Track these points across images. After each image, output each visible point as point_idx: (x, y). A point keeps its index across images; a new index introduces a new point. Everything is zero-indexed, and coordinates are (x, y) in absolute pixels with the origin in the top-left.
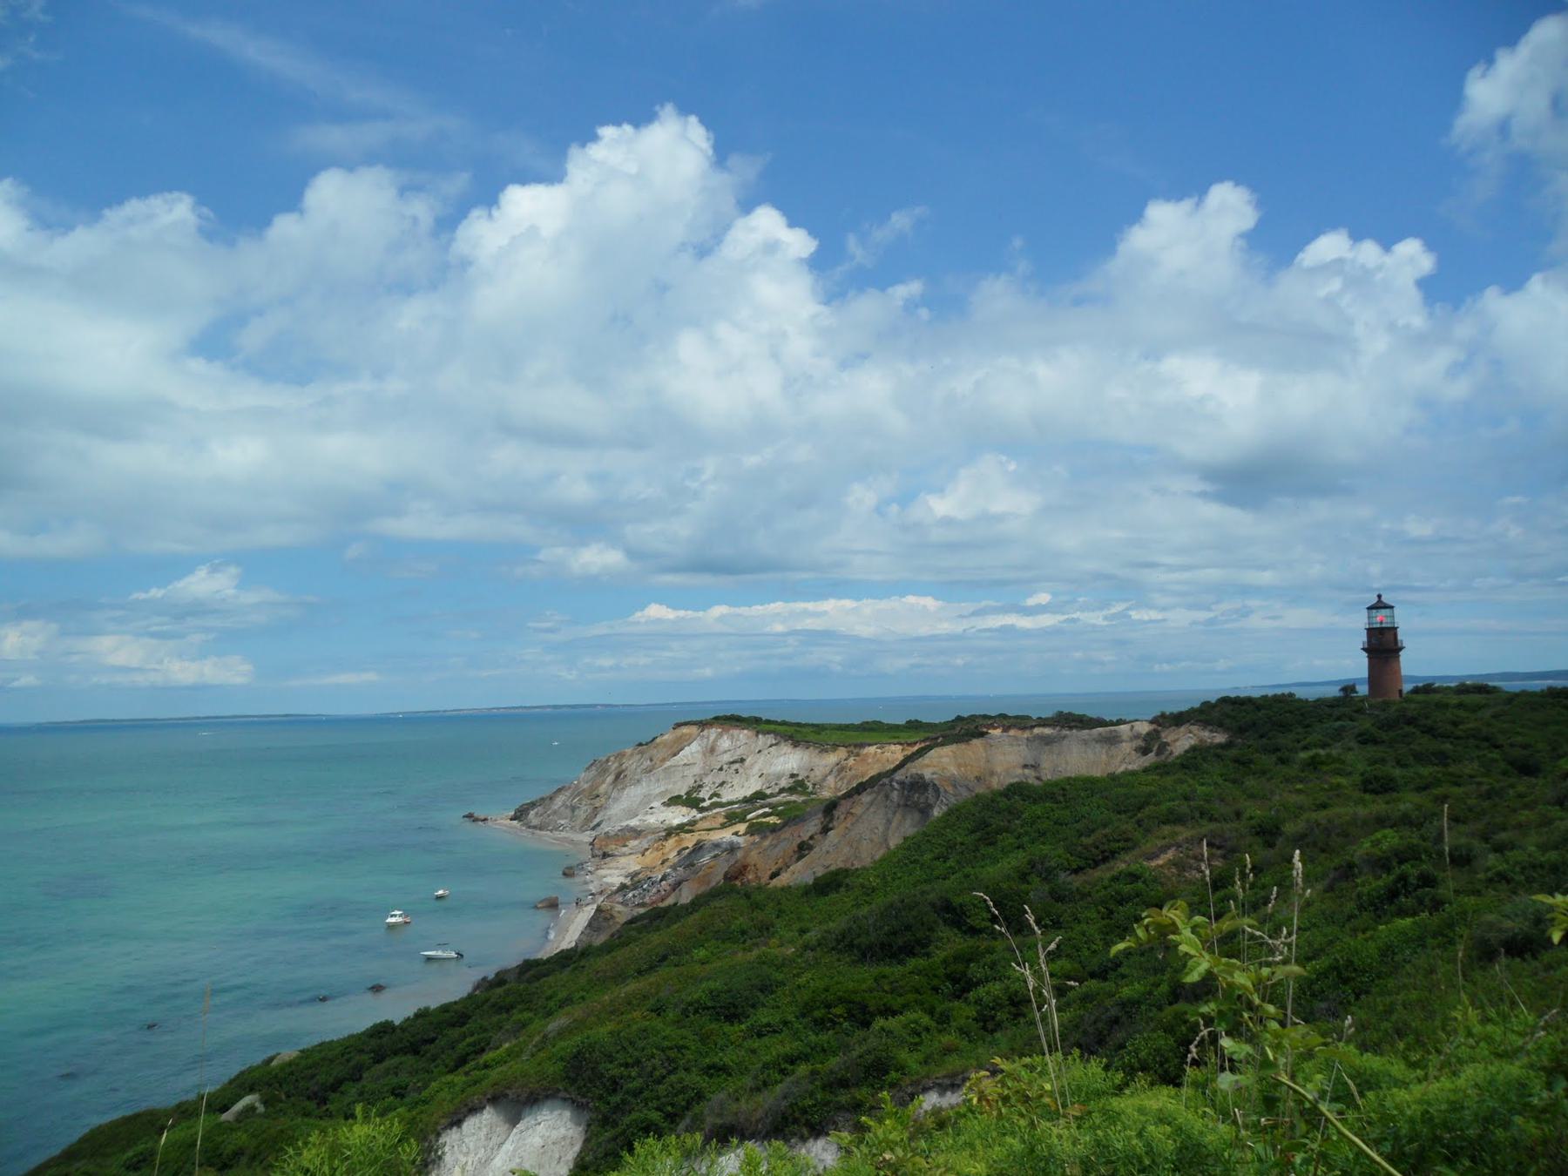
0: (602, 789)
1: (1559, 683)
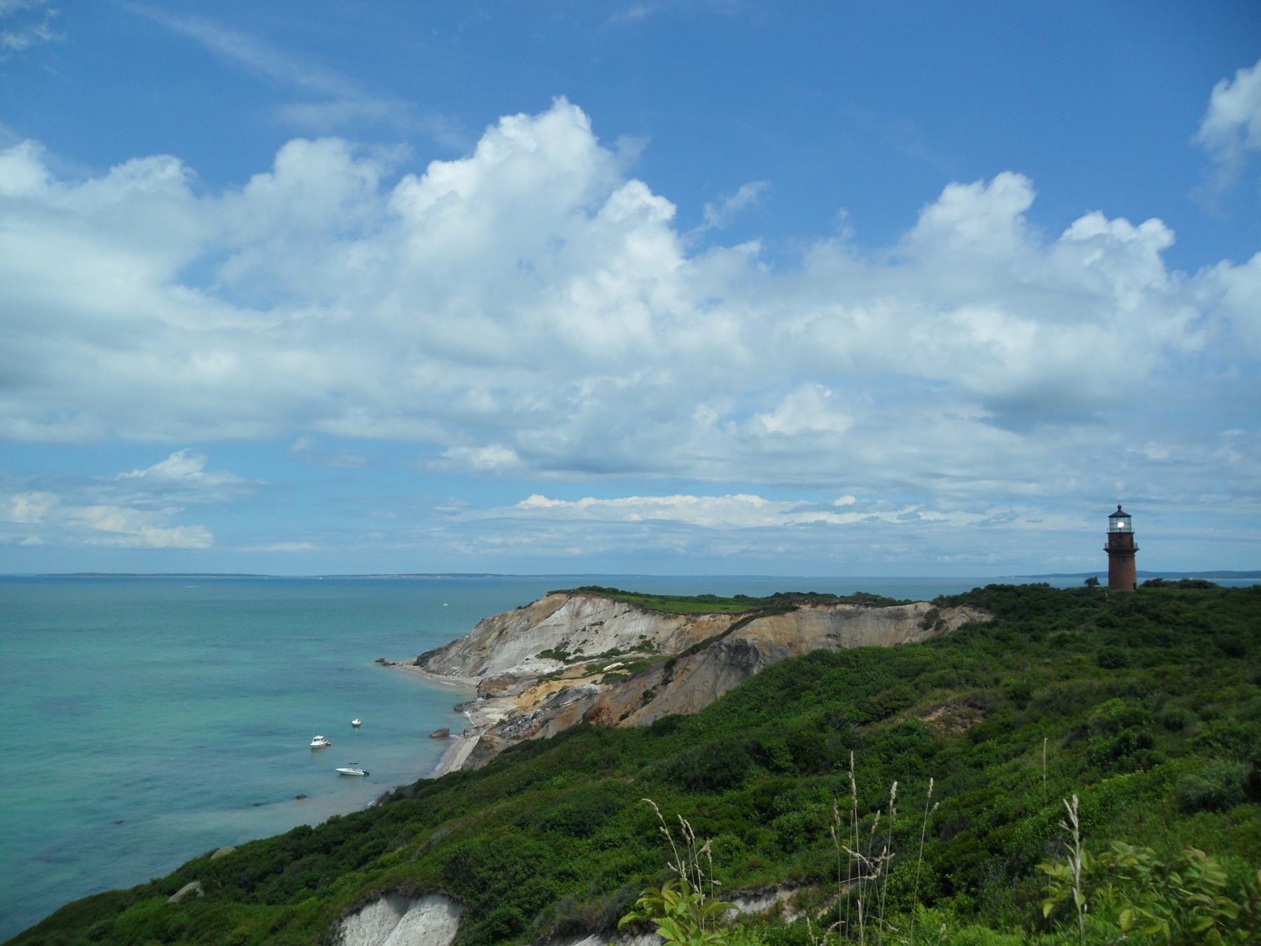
0: (488, 643)
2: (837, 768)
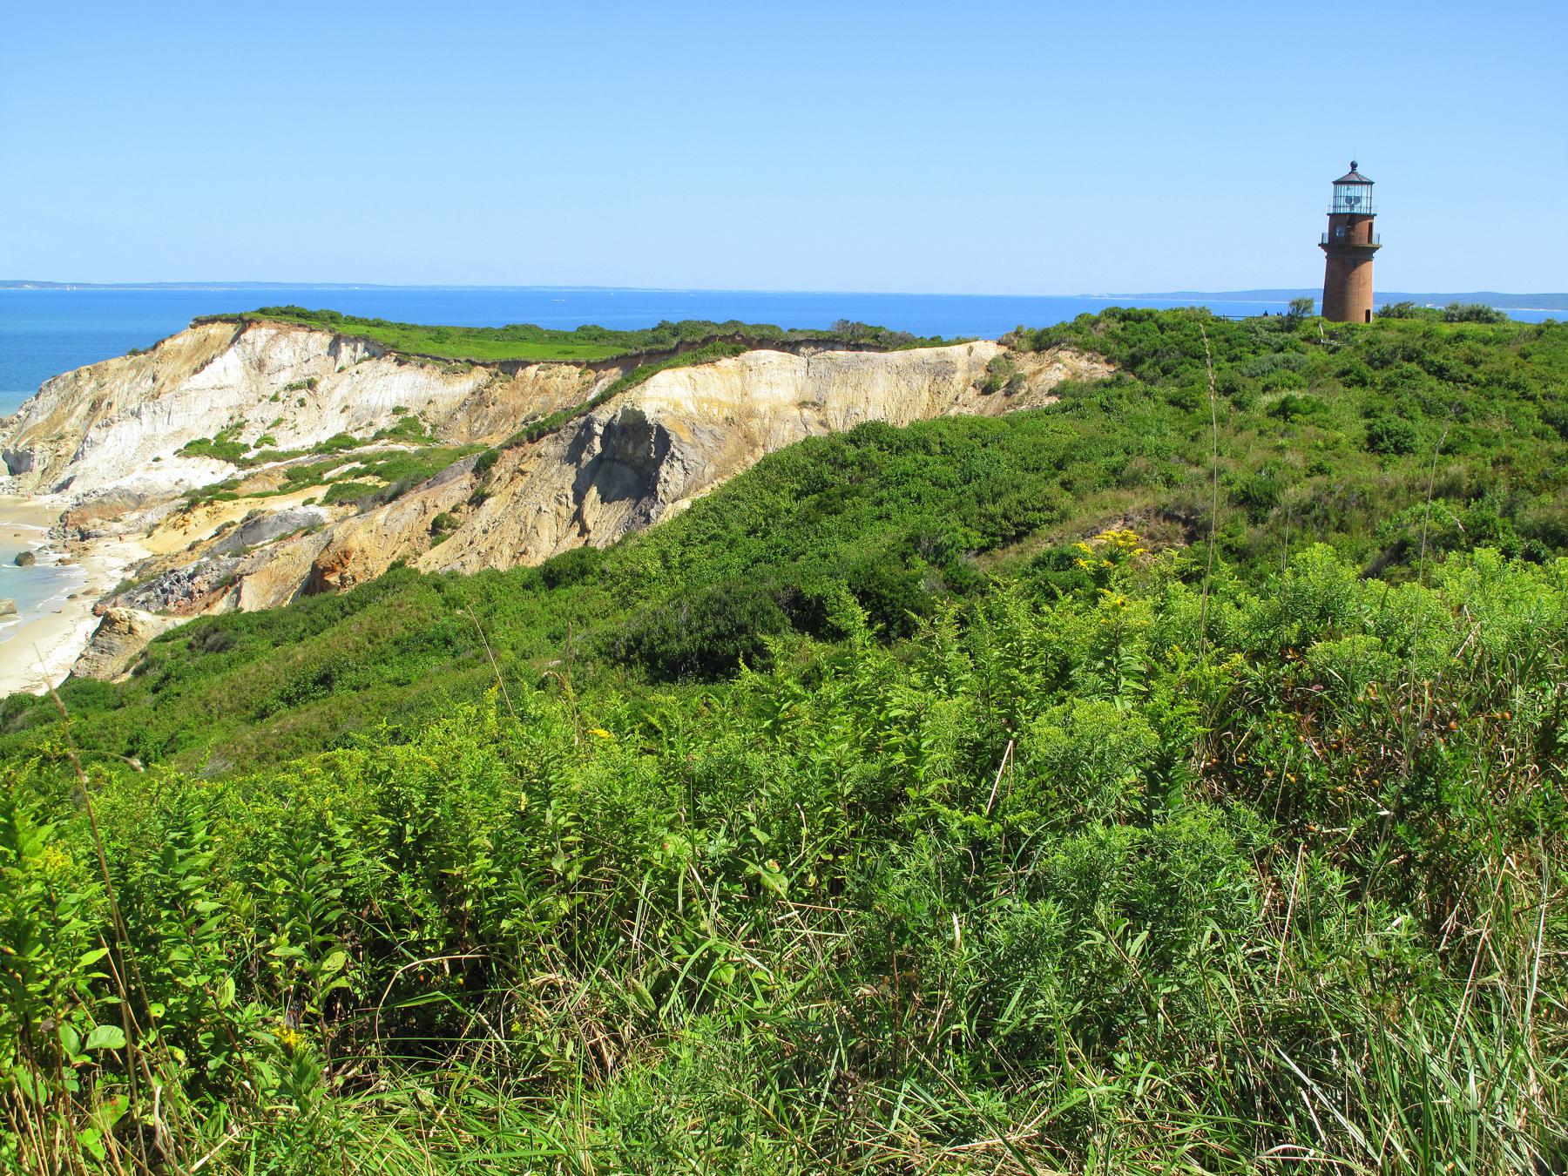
1: (1560, 315)
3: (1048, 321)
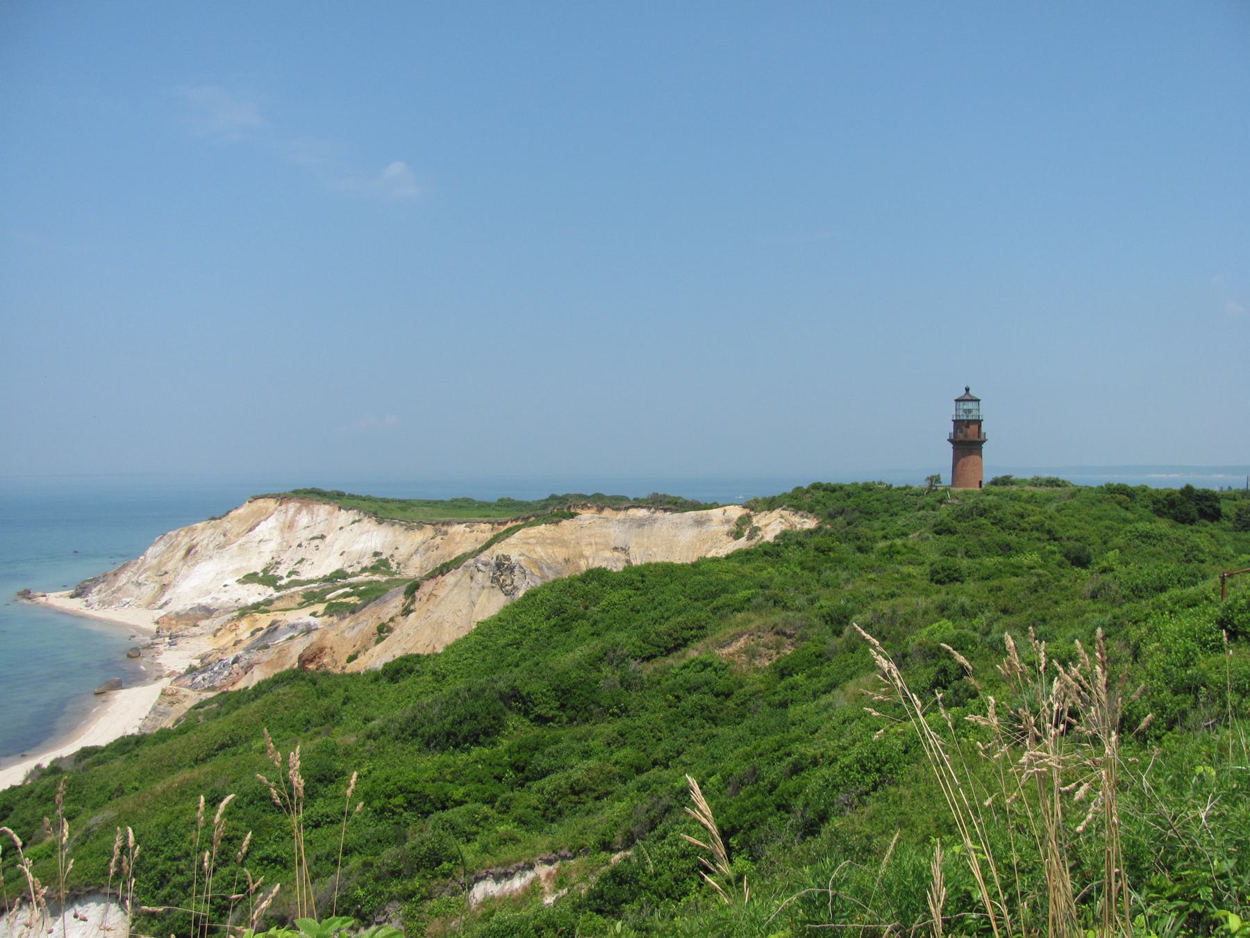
0: (170, 566)
2: (613, 714)
3: (777, 492)
